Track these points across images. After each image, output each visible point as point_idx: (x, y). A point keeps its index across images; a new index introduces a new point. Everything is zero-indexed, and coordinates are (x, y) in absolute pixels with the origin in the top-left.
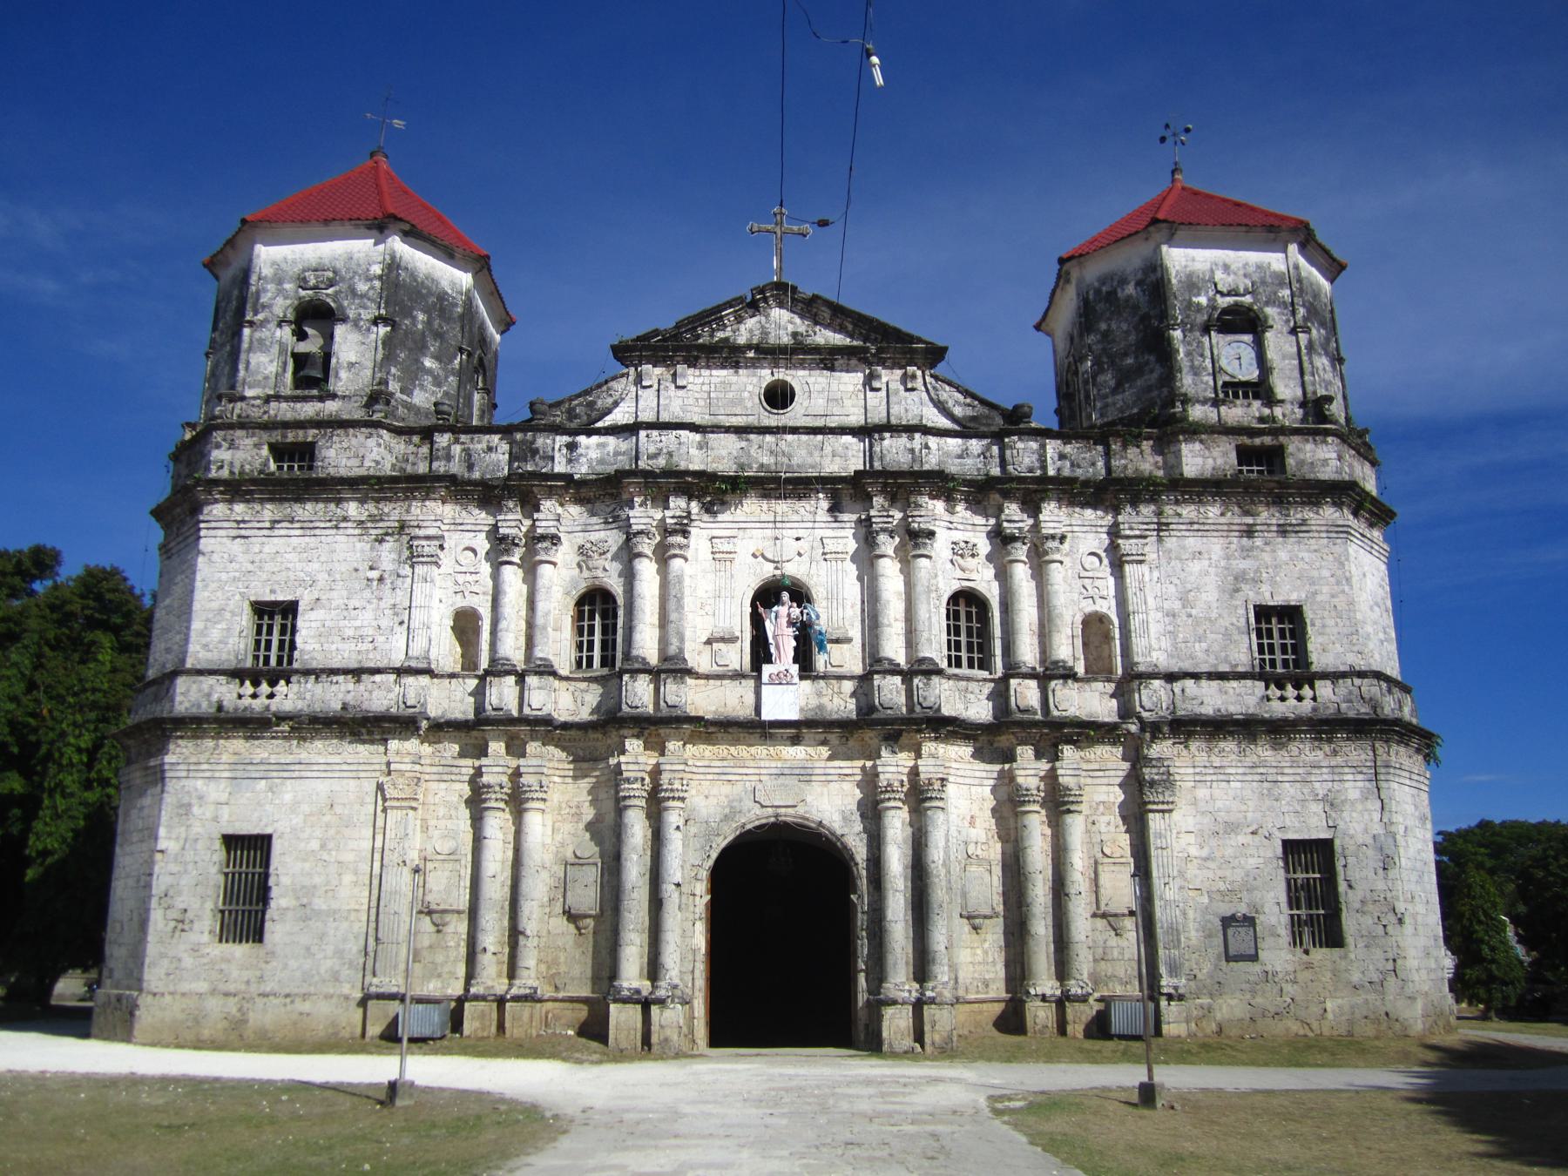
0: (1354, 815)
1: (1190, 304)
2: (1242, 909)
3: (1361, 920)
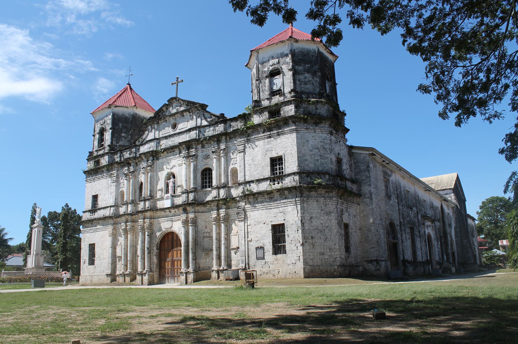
0: (290, 215)
1: (263, 71)
2: (261, 245)
3: (291, 246)
